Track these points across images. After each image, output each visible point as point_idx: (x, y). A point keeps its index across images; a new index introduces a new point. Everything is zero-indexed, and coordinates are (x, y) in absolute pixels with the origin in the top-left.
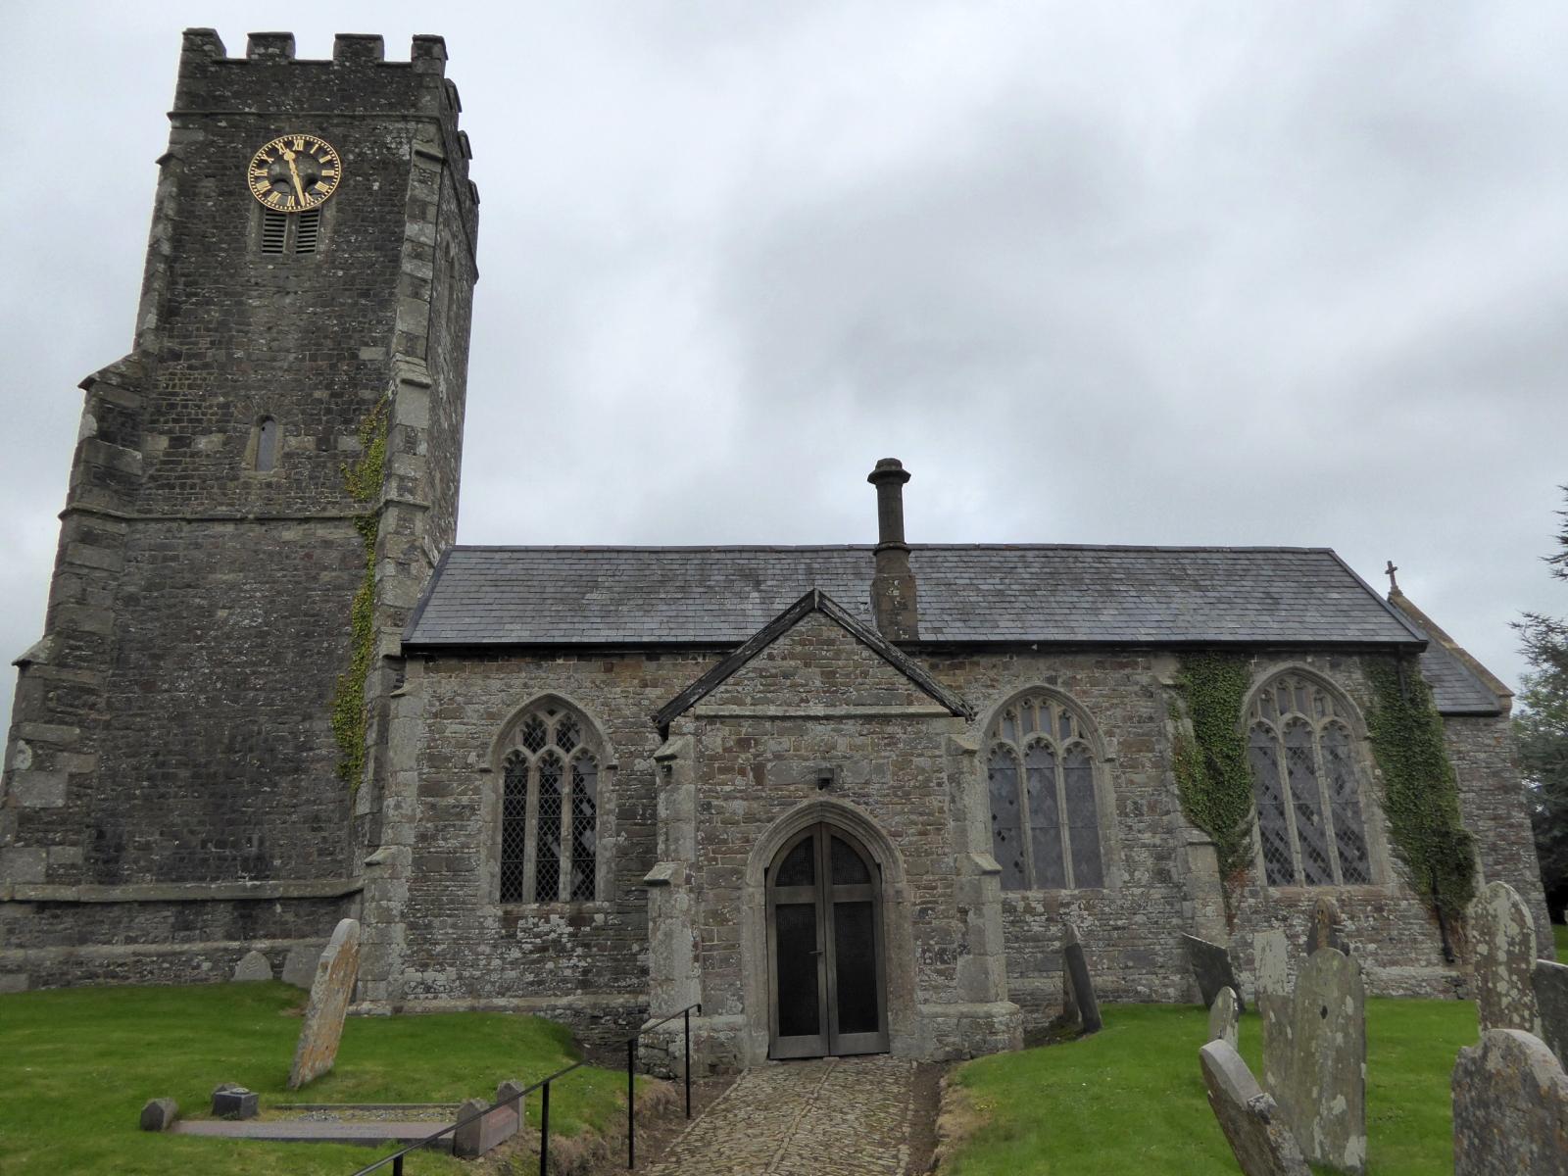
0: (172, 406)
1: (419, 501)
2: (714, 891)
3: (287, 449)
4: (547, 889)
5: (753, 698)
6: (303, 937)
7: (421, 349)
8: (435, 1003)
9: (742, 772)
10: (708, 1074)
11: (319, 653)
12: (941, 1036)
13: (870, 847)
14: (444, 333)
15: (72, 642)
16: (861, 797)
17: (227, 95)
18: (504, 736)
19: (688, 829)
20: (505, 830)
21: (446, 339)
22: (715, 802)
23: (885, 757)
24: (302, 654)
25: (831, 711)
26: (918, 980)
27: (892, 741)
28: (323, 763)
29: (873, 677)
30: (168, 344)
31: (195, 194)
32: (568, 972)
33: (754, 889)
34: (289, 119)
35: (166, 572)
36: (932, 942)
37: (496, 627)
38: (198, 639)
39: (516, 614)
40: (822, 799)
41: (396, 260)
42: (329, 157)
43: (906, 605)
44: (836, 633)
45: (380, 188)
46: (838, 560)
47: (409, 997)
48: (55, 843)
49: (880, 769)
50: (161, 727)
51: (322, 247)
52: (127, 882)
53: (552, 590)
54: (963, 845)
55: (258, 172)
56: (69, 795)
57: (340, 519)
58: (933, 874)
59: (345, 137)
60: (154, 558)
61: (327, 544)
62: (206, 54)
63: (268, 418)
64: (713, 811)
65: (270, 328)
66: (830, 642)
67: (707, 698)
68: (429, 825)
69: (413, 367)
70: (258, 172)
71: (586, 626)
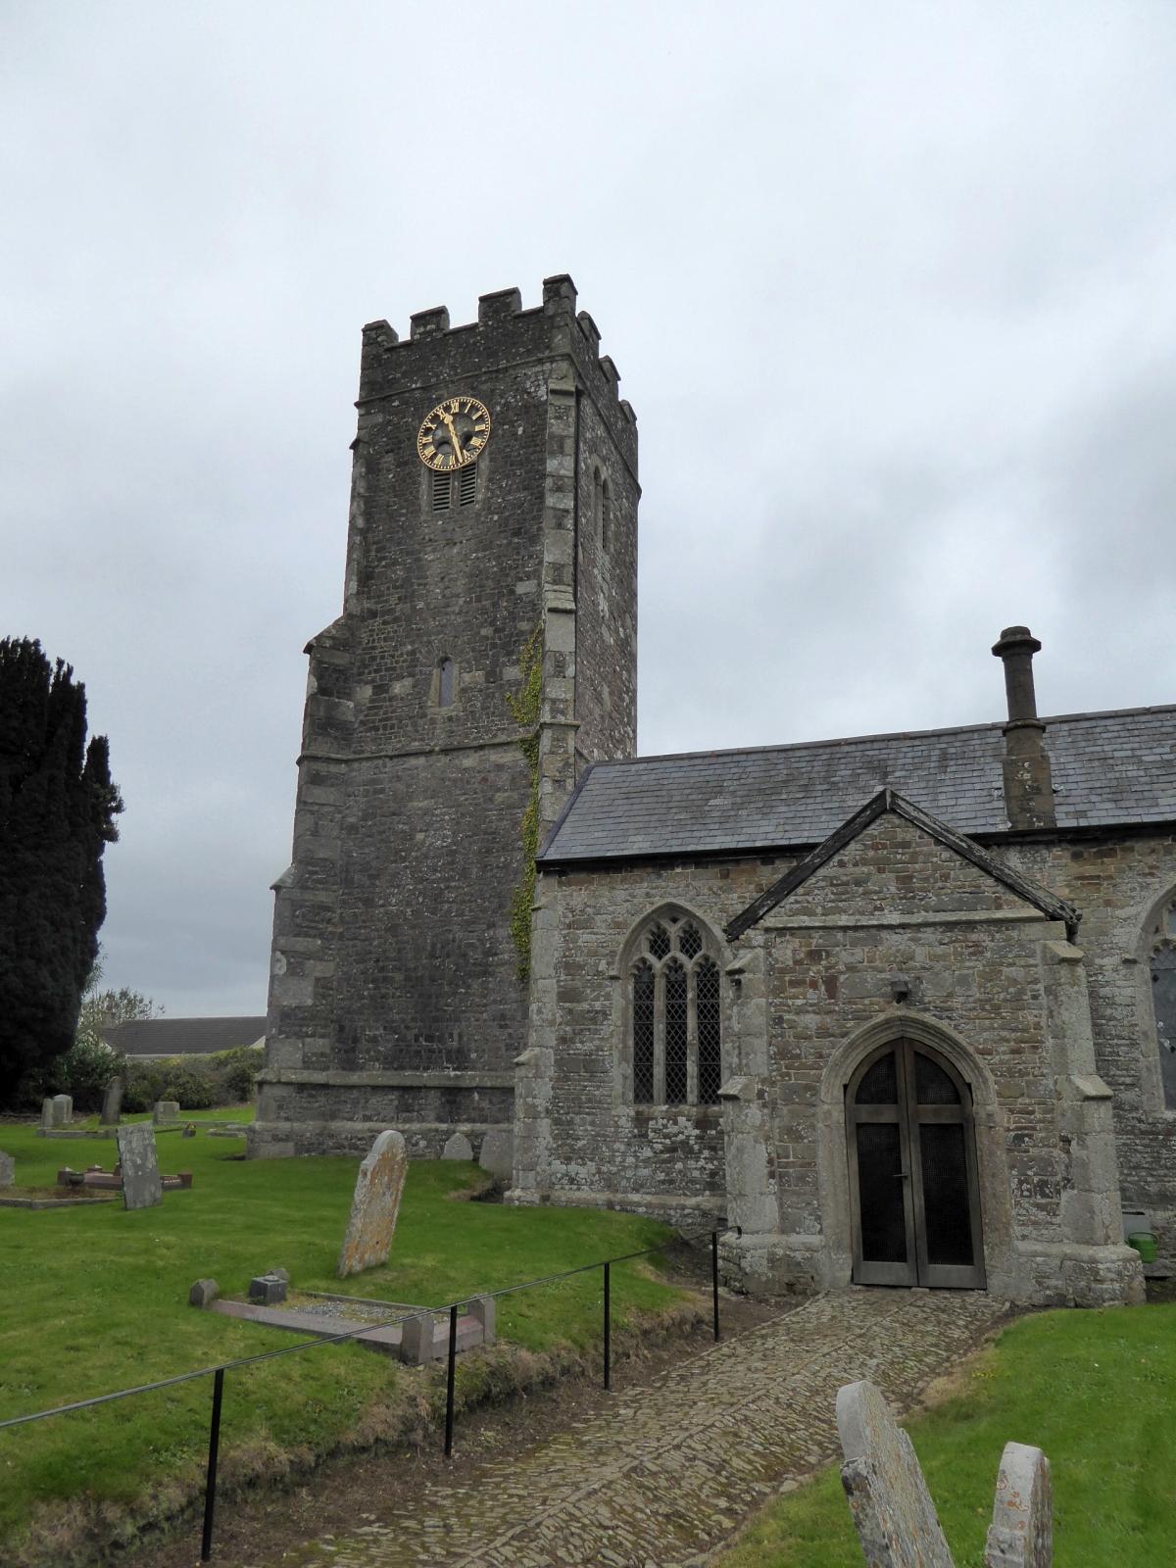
0: (373, 659)
1: (570, 720)
2: (789, 1107)
3: (462, 685)
4: (675, 1092)
5: (823, 907)
6: (497, 1122)
7: (568, 576)
8: (578, 1194)
9: (814, 985)
10: (784, 1292)
11: (498, 867)
12: (1041, 1279)
13: (959, 1066)
14: (600, 553)
15: (310, 868)
16: (944, 1011)
17: (403, 369)
18: (630, 944)
19: (760, 1044)
20: (636, 1033)
21: (603, 559)
22: (787, 1017)
23: (969, 968)
24: (485, 868)
25: (907, 919)
26: (1014, 1213)
27: (977, 950)
28: (506, 967)
29: (955, 880)
30: (367, 605)
31: (379, 471)
32: (696, 1174)
33: (831, 1108)
34: (447, 387)
35: (376, 803)
36: (1030, 1173)
37: (620, 840)
38: (404, 859)
39: (641, 825)
40: (899, 1013)
41: (541, 497)
42: (480, 413)
43: (1039, 789)
44: (912, 834)
45: (524, 431)
46: (978, 742)
47: (557, 1187)
48: (308, 1036)
49: (963, 981)
50: (380, 937)
51: (480, 497)
52: (362, 1069)
53: (678, 798)
54: (1063, 1067)
55: (425, 440)
56: (316, 995)
57: (508, 744)
58: (1029, 1097)
59: (492, 391)
60: (367, 791)
61: (499, 767)
62: (380, 344)
63: (446, 659)
64: (785, 1025)
65: (443, 578)
66: (905, 845)
67: (777, 909)
68: (568, 1029)
69: (559, 595)
70: (425, 440)
71: (702, 834)
